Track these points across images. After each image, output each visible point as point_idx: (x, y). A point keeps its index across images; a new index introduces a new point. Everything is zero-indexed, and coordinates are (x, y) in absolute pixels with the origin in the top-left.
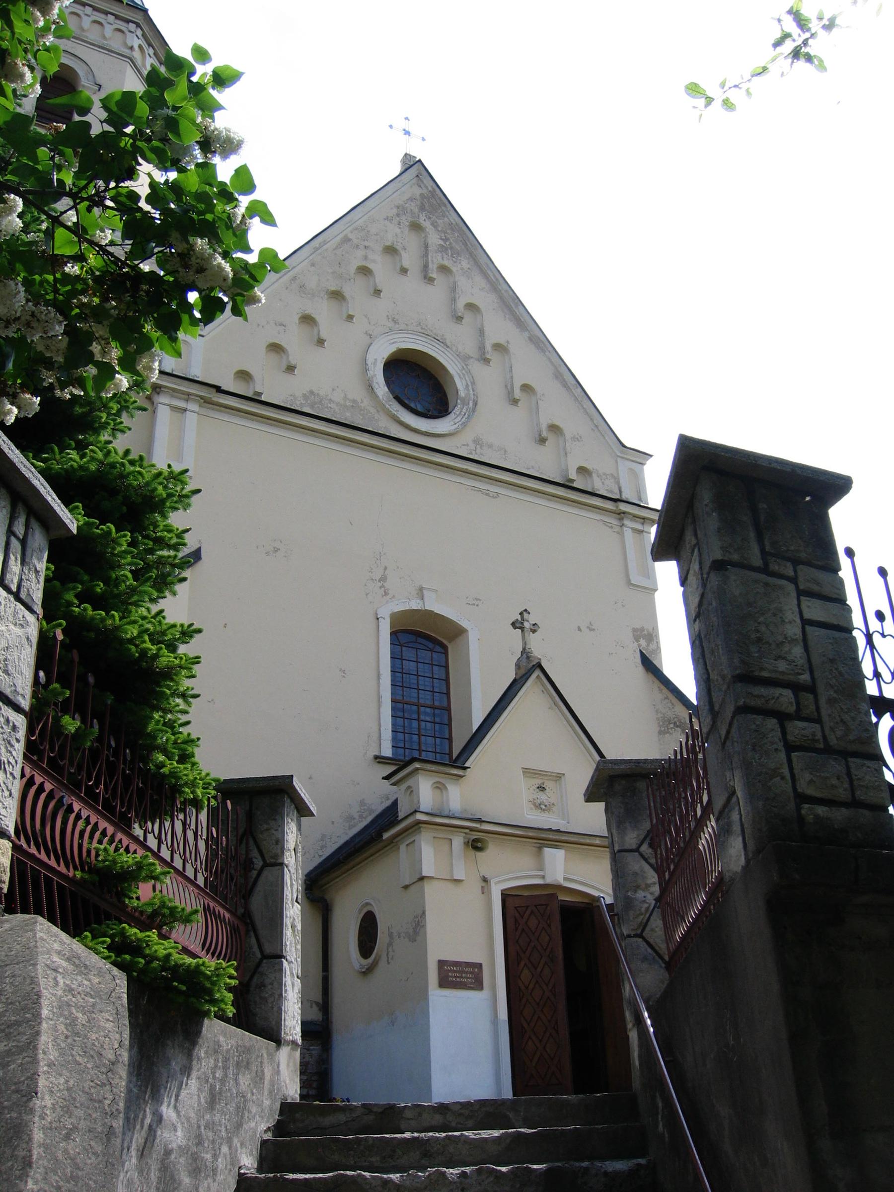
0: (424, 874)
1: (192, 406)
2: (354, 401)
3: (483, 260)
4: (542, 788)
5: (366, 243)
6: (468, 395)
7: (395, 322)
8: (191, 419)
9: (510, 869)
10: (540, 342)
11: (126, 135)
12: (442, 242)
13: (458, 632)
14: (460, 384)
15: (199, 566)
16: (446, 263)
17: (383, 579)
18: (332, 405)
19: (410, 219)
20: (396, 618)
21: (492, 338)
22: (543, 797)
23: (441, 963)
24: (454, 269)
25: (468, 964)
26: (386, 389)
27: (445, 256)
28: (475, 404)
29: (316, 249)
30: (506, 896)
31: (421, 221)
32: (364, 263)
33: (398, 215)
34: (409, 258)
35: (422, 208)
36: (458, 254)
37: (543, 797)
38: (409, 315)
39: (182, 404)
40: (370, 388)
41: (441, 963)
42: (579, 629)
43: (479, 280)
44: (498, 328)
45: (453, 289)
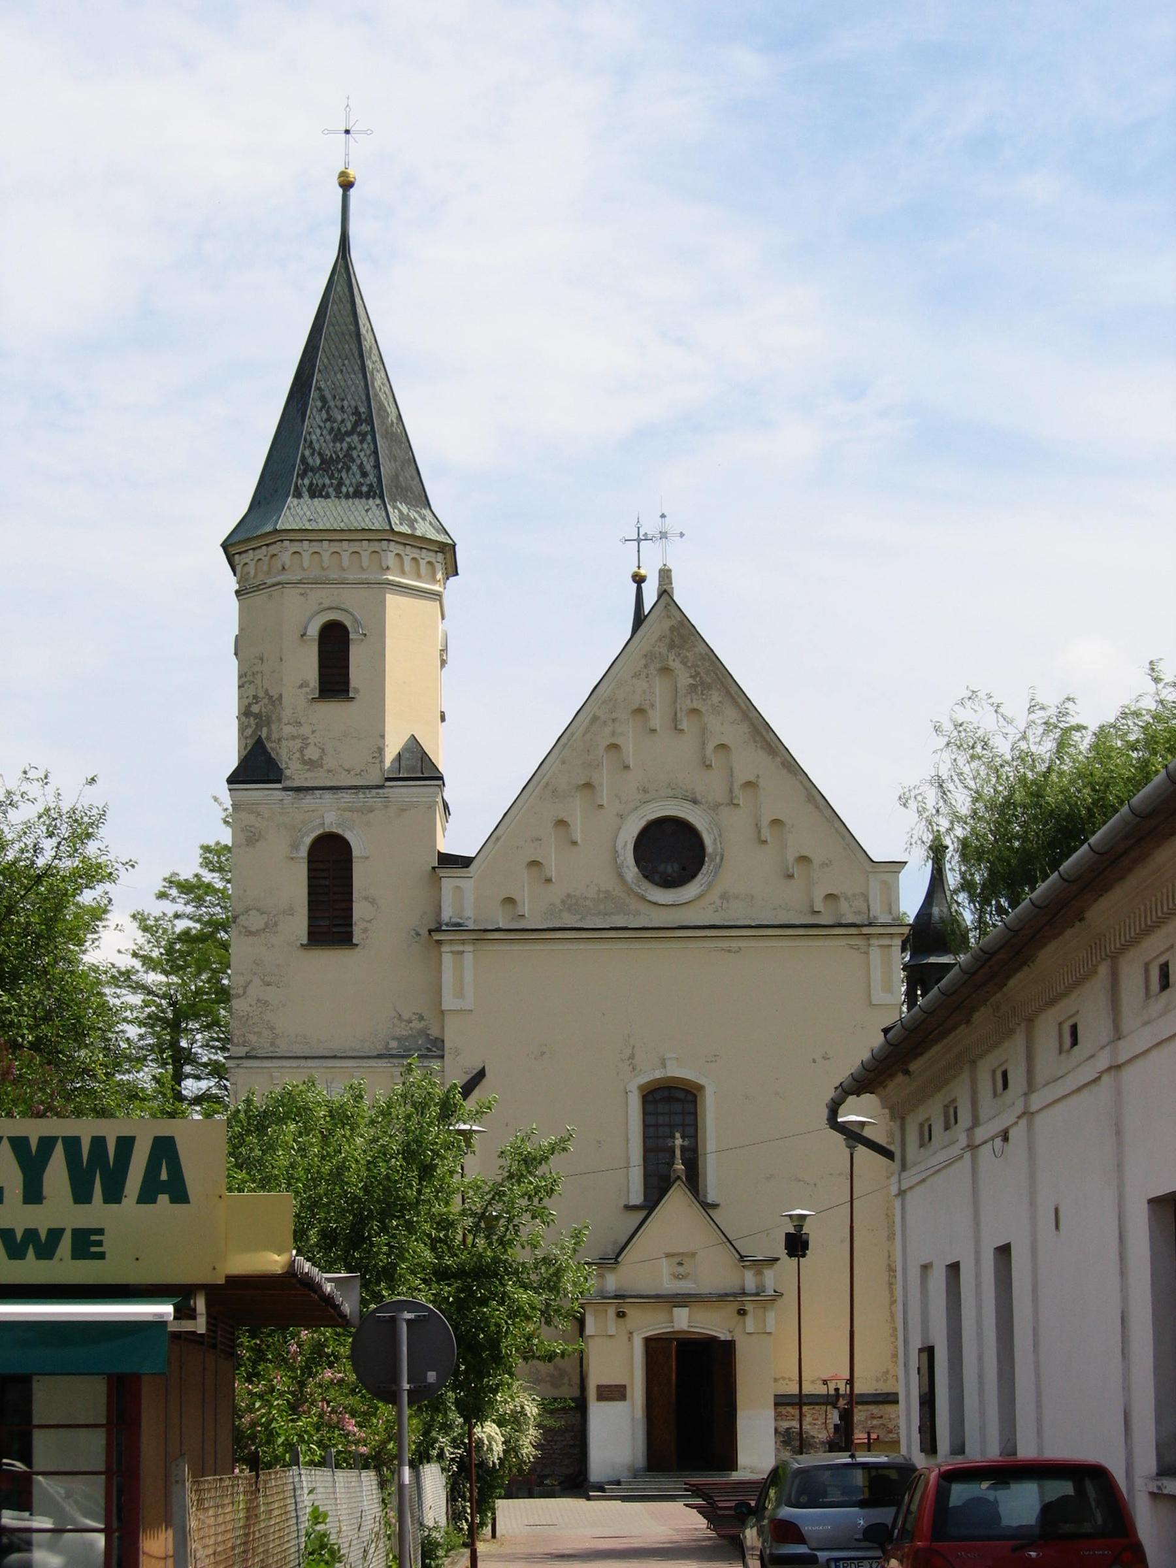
0: (369, 1478)
1: (468, 948)
2: (607, 892)
3: (733, 689)
4: (680, 1264)
5: (614, 715)
6: (715, 849)
7: (645, 791)
8: (468, 958)
9: (653, 1323)
10: (792, 766)
11: (116, 1530)
12: (691, 681)
13: (701, 1088)
14: (708, 840)
15: (485, 1081)
16: (695, 705)
17: (632, 1057)
18: (588, 903)
19: (658, 666)
20: (641, 1088)
21: (742, 777)
22: (681, 1270)
23: (599, 1387)
24: (703, 710)
25: (616, 1386)
26: (636, 869)
27: (695, 697)
28: (722, 859)
29: (564, 746)
30: (648, 1341)
31: (671, 663)
32: (613, 741)
33: (646, 666)
34: (657, 718)
35: (672, 646)
36: (709, 687)
37: (681, 1270)
38: (660, 777)
39: (461, 948)
40: (621, 876)
41: (599, 1387)
42: (814, 1061)
43: (731, 712)
44: (748, 762)
45: (703, 730)
